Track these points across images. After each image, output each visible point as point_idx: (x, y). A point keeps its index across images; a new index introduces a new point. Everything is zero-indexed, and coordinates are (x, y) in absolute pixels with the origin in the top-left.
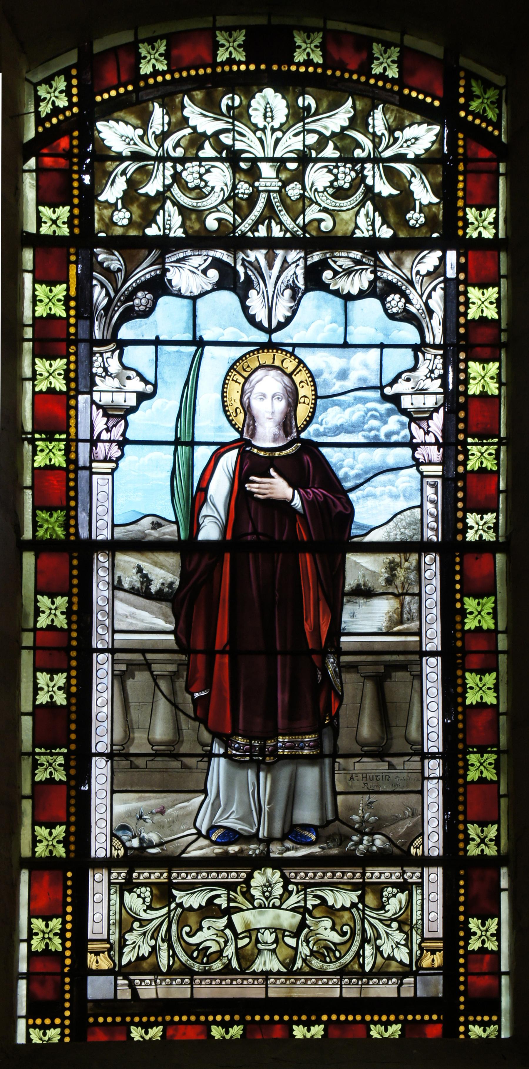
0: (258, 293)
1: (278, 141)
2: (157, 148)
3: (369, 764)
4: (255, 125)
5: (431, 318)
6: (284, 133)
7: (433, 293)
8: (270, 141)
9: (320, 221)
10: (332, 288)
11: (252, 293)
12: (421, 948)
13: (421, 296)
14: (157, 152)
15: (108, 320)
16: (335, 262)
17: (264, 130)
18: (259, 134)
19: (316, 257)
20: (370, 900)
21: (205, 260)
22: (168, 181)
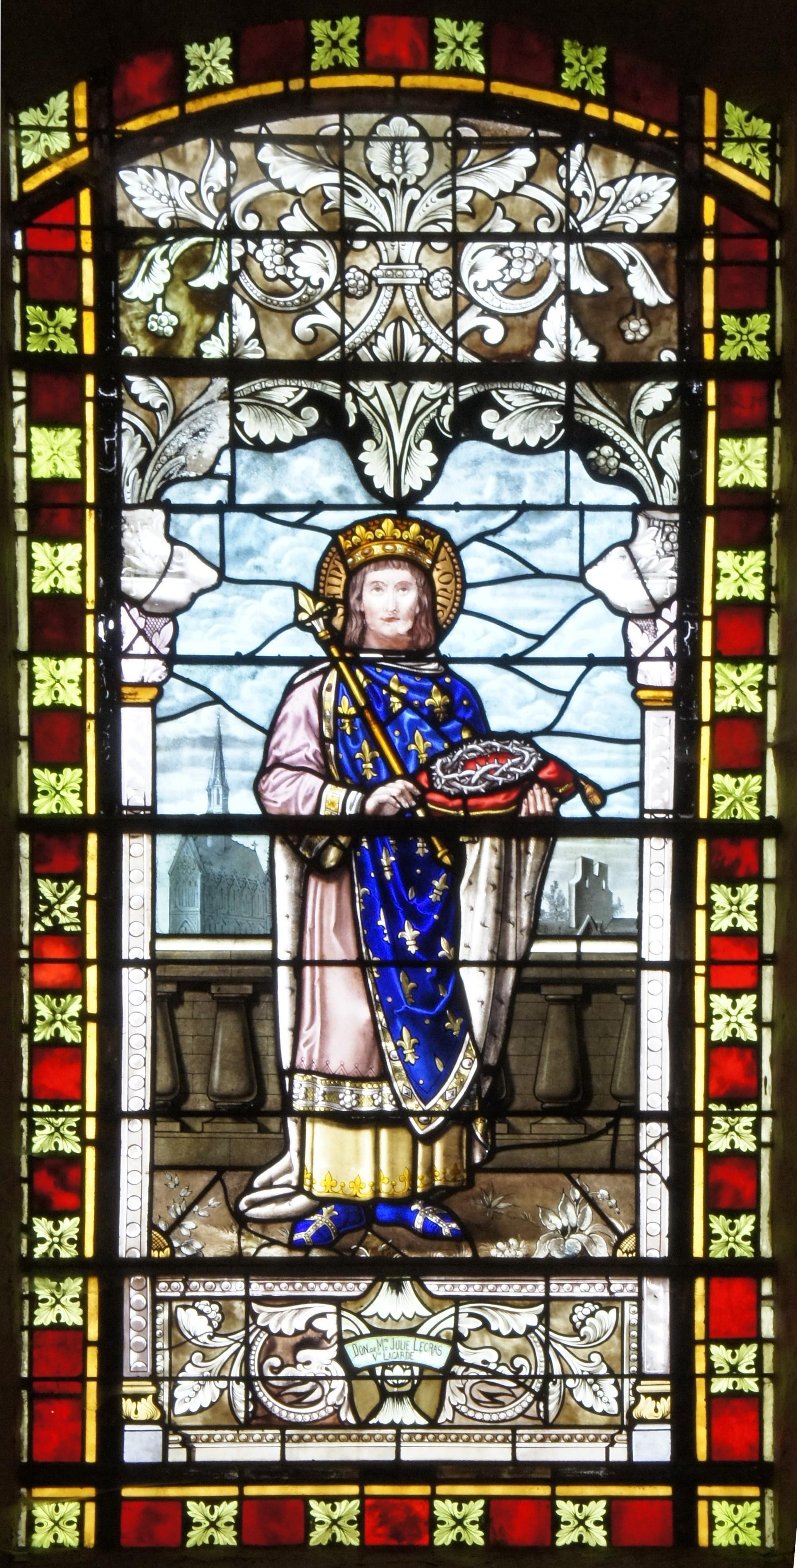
0: (378, 446)
1: (413, 204)
2: (216, 214)
3: (554, 1126)
4: (378, 179)
5: (660, 481)
6: (423, 192)
7: (663, 443)
8: (400, 207)
9: (480, 330)
10: (496, 436)
11: (368, 444)
12: (637, 1395)
13: (645, 448)
14: (217, 221)
15: (146, 485)
16: (502, 396)
17: (391, 186)
18: (384, 192)
19: (467, 391)
20: (558, 1322)
21: (296, 394)
22: (236, 266)
